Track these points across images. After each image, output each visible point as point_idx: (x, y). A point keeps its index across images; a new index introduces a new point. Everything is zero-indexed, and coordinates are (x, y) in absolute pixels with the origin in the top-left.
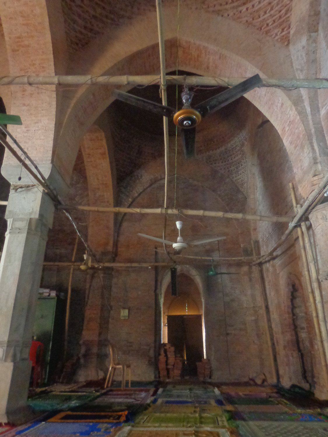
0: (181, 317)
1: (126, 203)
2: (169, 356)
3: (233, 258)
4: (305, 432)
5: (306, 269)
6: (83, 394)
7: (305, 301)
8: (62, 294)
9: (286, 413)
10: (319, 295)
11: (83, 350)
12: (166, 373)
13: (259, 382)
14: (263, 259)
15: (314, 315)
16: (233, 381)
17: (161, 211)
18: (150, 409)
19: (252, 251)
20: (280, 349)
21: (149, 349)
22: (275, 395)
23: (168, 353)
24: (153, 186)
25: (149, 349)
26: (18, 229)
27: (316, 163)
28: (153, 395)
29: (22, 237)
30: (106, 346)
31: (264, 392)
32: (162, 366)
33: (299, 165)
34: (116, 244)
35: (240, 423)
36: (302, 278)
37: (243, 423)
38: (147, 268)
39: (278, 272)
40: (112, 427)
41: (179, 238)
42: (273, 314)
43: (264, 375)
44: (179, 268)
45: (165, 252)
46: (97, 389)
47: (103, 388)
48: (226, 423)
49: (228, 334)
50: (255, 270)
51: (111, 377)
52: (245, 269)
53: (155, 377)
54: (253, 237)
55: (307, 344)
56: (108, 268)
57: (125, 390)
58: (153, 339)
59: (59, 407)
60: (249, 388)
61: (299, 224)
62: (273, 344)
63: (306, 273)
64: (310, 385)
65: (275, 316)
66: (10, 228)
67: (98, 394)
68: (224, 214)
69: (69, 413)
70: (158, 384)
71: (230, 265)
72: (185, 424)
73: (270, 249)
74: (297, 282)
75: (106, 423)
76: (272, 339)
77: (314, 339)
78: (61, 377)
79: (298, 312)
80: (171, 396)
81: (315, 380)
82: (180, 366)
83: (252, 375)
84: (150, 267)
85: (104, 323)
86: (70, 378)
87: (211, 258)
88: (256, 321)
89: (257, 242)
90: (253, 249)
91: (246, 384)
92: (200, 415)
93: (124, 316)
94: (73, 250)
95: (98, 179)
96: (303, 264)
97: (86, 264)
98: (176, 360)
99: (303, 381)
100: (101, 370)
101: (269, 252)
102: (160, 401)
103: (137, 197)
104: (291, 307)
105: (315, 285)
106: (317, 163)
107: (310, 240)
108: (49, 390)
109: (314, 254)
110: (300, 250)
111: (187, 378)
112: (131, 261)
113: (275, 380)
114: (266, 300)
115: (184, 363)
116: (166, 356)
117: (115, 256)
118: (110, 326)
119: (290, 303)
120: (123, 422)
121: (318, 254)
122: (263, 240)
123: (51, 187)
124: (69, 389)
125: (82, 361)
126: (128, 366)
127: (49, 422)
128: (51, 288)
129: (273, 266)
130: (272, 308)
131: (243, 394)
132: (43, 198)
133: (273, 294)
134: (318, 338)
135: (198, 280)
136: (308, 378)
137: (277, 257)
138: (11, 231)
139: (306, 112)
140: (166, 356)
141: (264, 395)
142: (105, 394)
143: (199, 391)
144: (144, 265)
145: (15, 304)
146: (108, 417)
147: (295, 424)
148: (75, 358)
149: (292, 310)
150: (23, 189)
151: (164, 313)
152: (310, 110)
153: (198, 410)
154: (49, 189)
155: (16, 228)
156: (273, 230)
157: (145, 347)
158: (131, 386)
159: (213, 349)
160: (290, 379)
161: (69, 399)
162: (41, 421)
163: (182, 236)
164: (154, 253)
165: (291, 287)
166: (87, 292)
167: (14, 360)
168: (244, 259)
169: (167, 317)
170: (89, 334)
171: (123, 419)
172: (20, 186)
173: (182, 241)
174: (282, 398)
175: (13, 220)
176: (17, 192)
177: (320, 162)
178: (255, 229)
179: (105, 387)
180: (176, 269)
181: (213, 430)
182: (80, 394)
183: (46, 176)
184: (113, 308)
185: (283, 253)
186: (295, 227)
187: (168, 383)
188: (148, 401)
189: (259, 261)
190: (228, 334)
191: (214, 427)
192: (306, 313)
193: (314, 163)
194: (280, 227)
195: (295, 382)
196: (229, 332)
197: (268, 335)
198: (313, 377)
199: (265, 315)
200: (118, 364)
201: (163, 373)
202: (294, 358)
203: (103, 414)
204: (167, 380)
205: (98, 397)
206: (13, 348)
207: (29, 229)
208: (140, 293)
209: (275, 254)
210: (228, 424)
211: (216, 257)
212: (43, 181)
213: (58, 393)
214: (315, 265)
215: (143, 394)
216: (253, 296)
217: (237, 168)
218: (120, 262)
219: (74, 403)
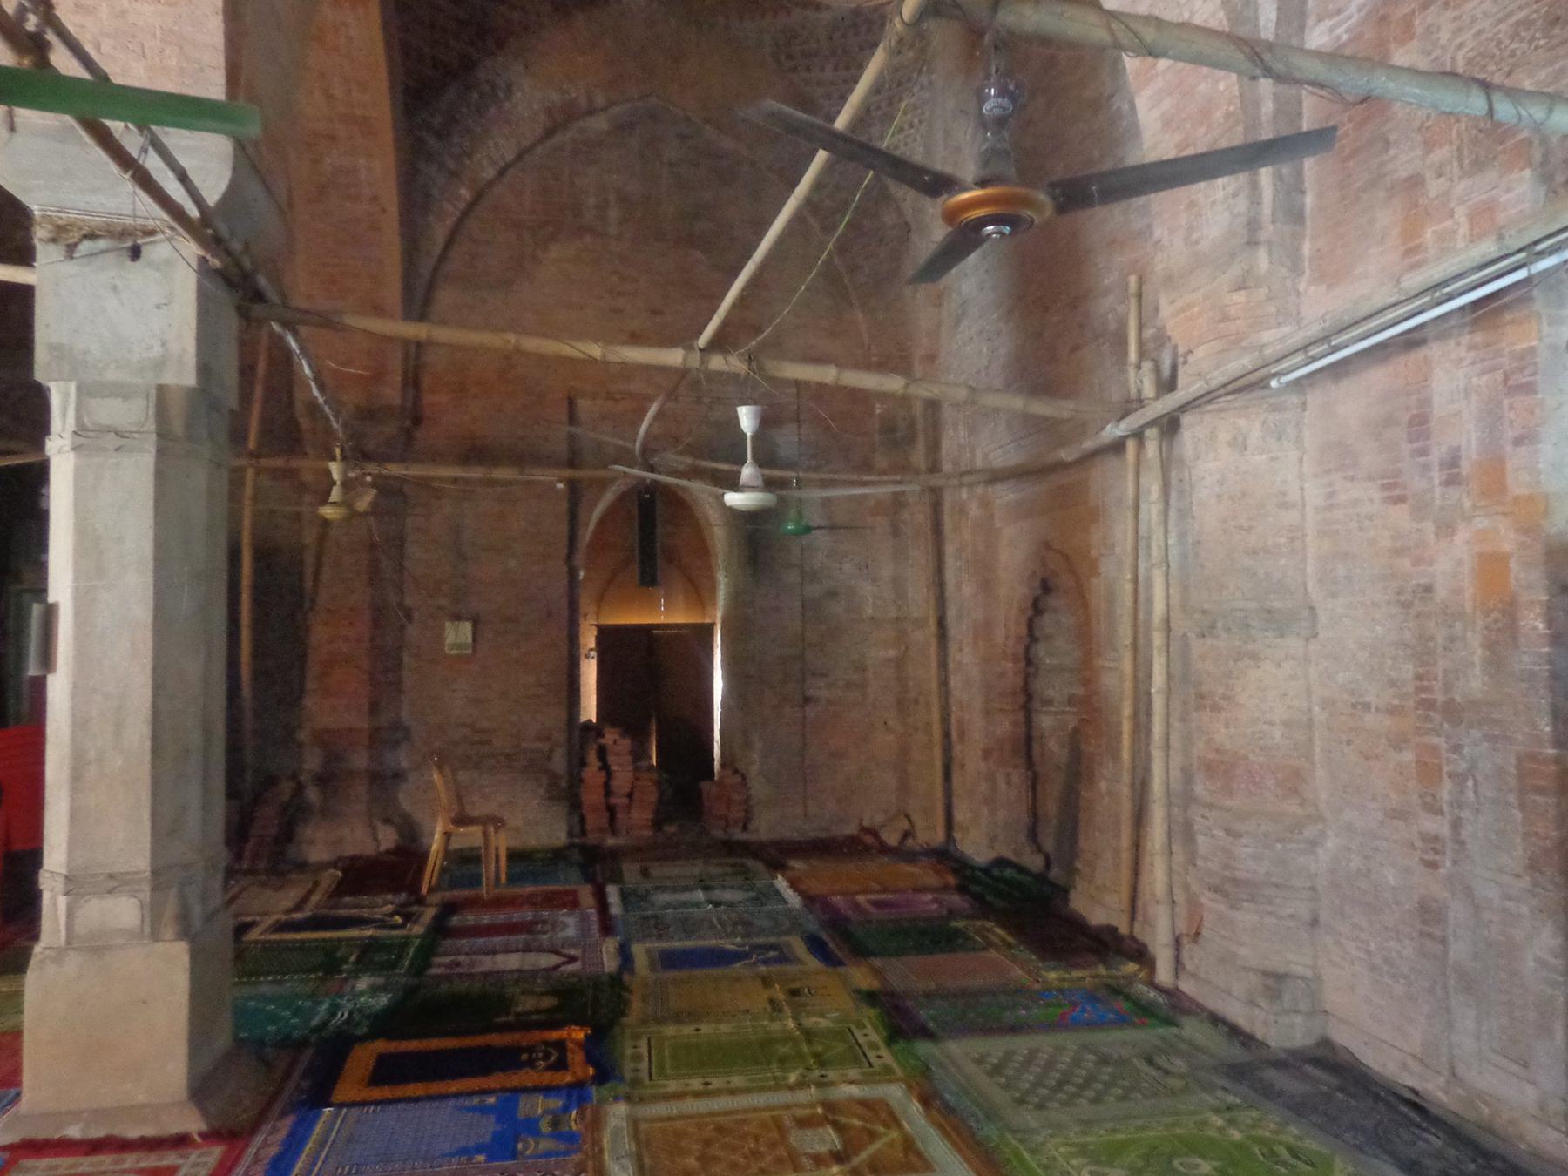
0: (646, 630)
1: (448, 207)
2: (614, 768)
11: (312, 761)
12: (604, 822)
17: (685, 359)
20: (971, 762)
21: (551, 751)
23: (611, 759)
24: (558, 139)
25: (551, 751)
27: (1253, 243)
30: (396, 744)
31: (929, 893)
32: (592, 797)
33: (1183, 219)
41: (748, 472)
42: (961, 650)
43: (908, 817)
49: (807, 700)
53: (570, 834)
58: (564, 715)
68: (907, 385)
78: (247, 853)
79: (1042, 654)
83: (873, 818)
84: (560, 486)
85: (385, 671)
88: (900, 663)
90: (920, 425)
93: (459, 646)
95: (329, 97)
100: (387, 821)
103: (490, 184)
106: (1257, 243)
113: (939, 837)
116: (605, 767)
118: (408, 678)
119: (1024, 631)
123: (237, 246)
125: (313, 795)
129: (985, 503)
132: (203, 297)
133: (968, 590)
138: (81, 440)
139: (1257, 19)
140: (605, 767)
145: (155, 738)
148: (286, 788)
149: (1027, 649)
150: (102, 244)
152: (1273, 16)
154: (228, 252)
157: (538, 745)
159: (759, 745)
160: (992, 840)
165: (1037, 584)
166: (309, 559)
167: (185, 933)
172: (86, 231)
174: (987, 919)
175: (79, 389)
176: (76, 255)
177: (1270, 243)
183: (212, 197)
184: (416, 615)
193: (1248, 243)
196: (811, 692)
199: (933, 651)
201: (595, 821)
202: (1011, 786)
204: (611, 841)
206: (174, 891)
207: (163, 434)
208: (513, 564)
212: (194, 212)
216: (898, 584)
217: (890, 104)
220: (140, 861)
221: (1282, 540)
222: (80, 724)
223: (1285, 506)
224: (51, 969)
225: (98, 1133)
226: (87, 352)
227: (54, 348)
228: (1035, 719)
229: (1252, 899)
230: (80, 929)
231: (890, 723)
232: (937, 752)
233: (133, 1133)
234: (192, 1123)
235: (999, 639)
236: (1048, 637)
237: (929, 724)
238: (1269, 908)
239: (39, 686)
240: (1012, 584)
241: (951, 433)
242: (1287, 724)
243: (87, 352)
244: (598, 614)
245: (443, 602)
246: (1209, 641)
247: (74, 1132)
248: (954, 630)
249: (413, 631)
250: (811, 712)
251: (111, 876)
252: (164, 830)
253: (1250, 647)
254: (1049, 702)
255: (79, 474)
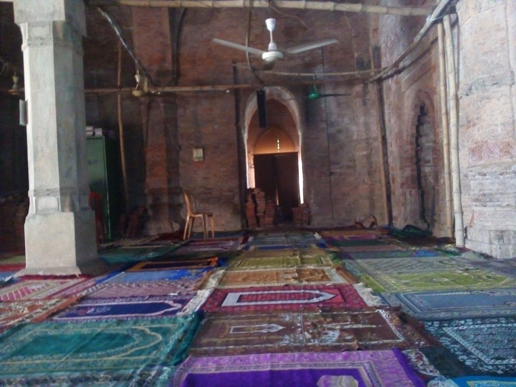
0: (272, 156)
2: (258, 202)
3: (344, 74)
4: (418, 265)
5: (442, 83)
6: (159, 246)
7: (435, 126)
8: (111, 132)
9: (398, 251)
10: (455, 116)
11: (150, 201)
13: (367, 225)
14: (385, 73)
15: (445, 141)
16: (336, 226)
18: (243, 255)
19: (369, 62)
20: (397, 190)
21: (234, 196)
22: (385, 236)
26: (40, 40)
28: (243, 243)
29: (48, 51)
31: (373, 235)
32: (250, 213)
34: (176, 59)
35: (347, 262)
36: (435, 96)
37: (351, 261)
38: (224, 92)
39: (403, 91)
40: (203, 271)
41: (271, 45)
42: (391, 146)
43: (374, 217)
44: (267, 90)
45: (249, 68)
46: (174, 241)
47: (182, 240)
48: (331, 262)
49: (331, 174)
50: (372, 89)
51: (190, 230)
52: (358, 88)
54: (372, 42)
55: (431, 180)
56: (168, 94)
57: (209, 241)
59: (135, 259)
60: (356, 232)
61: (441, 17)
62: (388, 183)
63: (442, 88)
64: (428, 225)
65: (393, 148)
66: (27, 37)
67: (177, 245)
68: (335, 6)
69: (149, 263)
70: (246, 233)
71: (337, 84)
72: (285, 265)
73: (396, 57)
74: (427, 102)
75: (195, 268)
76: (387, 176)
77: (441, 172)
79: (424, 142)
80: (263, 243)
81: (436, 218)
82: (273, 212)
83: (359, 218)
84: (228, 91)
85: (173, 167)
86: (139, 231)
87: (313, 75)
88: (368, 157)
89: (377, 49)
91: (352, 228)
92: (300, 257)
93: (199, 158)
94: (116, 70)
96: (439, 77)
97: (140, 88)
98: (266, 206)
99: (420, 221)
100: (176, 221)
101: (394, 62)
102: (252, 248)
104: (416, 135)
105: (452, 103)
107: (452, 41)
108: (116, 245)
109: (456, 59)
110: (437, 58)
111: (281, 225)
112: (200, 83)
113: (386, 222)
114: (383, 129)
115: (276, 210)
116: (255, 202)
117: (177, 76)
118: (182, 171)
119: (415, 131)
120: (214, 267)
121: (461, 61)
122: (387, 45)
124: (141, 242)
125: (150, 213)
126: (210, 215)
127: (130, 272)
128: (96, 125)
129: (398, 83)
130: (390, 139)
131: (349, 238)
133: (393, 120)
134: (446, 170)
135: (294, 107)
136: (426, 218)
137: (404, 69)
140: (255, 202)
141: (374, 237)
142: (186, 245)
143: (297, 238)
144: (221, 88)
146: (198, 264)
147: (409, 259)
149: (417, 139)
151: (249, 152)
153: (298, 252)
155: (37, 38)
156: (402, 29)
157: (228, 194)
158: (215, 237)
159: (313, 192)
160: (406, 220)
161: (144, 251)
162: (120, 271)
163: (275, 41)
164: (232, 70)
165: (419, 110)
167: (73, 208)
168: (359, 73)
169: (252, 157)
170: (155, 181)
171: (213, 264)
173: (275, 49)
175: (29, 25)
178: (376, 30)
179: (184, 238)
180: (263, 92)
181: (317, 268)
182: (156, 246)
184: (183, 148)
185: (413, 63)
186: (435, 23)
187: (258, 232)
188: (239, 248)
189: (378, 76)
190: (331, 174)
191: (318, 266)
192: (435, 142)
194: (411, 24)
195: (410, 222)
196: (333, 171)
197: (383, 173)
198: (433, 214)
199: (380, 148)
200: (197, 213)
201: (252, 221)
203: (189, 261)
204: (257, 229)
205: (178, 248)
207: (56, 39)
208: (216, 127)
209: (401, 65)
210: (334, 263)
211: (319, 73)
213: (129, 247)
214: (455, 78)
215: (231, 243)
218: (186, 86)
219: (151, 255)
220: (56, 185)
221: (498, 45)
222: (35, 139)
223: (498, 30)
224: (31, 221)
225: (48, 274)
226: (30, 12)
227: (20, 11)
228: (422, 169)
229: (491, 201)
230: (40, 208)
231: (366, 181)
232: (384, 189)
233: (58, 274)
234: (77, 272)
235: (405, 138)
236: (427, 135)
237: (381, 179)
238: (499, 203)
239: (24, 129)
240: (409, 112)
241: (384, 59)
242: (503, 124)
243: (30, 12)
244: (254, 151)
245: (192, 142)
246: (470, 96)
247: (41, 273)
248: (389, 141)
249: (182, 153)
250: (333, 178)
251: (48, 190)
252: (64, 174)
253: (486, 94)
254: (429, 162)
255: (30, 55)
